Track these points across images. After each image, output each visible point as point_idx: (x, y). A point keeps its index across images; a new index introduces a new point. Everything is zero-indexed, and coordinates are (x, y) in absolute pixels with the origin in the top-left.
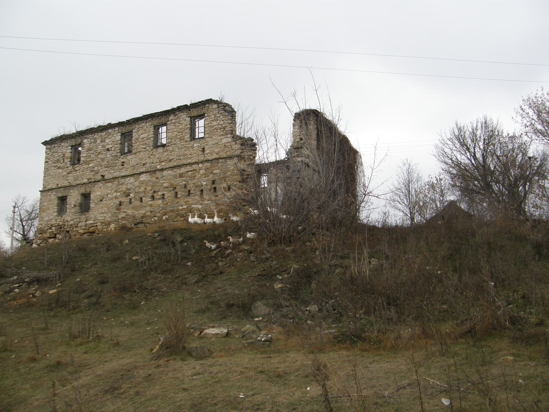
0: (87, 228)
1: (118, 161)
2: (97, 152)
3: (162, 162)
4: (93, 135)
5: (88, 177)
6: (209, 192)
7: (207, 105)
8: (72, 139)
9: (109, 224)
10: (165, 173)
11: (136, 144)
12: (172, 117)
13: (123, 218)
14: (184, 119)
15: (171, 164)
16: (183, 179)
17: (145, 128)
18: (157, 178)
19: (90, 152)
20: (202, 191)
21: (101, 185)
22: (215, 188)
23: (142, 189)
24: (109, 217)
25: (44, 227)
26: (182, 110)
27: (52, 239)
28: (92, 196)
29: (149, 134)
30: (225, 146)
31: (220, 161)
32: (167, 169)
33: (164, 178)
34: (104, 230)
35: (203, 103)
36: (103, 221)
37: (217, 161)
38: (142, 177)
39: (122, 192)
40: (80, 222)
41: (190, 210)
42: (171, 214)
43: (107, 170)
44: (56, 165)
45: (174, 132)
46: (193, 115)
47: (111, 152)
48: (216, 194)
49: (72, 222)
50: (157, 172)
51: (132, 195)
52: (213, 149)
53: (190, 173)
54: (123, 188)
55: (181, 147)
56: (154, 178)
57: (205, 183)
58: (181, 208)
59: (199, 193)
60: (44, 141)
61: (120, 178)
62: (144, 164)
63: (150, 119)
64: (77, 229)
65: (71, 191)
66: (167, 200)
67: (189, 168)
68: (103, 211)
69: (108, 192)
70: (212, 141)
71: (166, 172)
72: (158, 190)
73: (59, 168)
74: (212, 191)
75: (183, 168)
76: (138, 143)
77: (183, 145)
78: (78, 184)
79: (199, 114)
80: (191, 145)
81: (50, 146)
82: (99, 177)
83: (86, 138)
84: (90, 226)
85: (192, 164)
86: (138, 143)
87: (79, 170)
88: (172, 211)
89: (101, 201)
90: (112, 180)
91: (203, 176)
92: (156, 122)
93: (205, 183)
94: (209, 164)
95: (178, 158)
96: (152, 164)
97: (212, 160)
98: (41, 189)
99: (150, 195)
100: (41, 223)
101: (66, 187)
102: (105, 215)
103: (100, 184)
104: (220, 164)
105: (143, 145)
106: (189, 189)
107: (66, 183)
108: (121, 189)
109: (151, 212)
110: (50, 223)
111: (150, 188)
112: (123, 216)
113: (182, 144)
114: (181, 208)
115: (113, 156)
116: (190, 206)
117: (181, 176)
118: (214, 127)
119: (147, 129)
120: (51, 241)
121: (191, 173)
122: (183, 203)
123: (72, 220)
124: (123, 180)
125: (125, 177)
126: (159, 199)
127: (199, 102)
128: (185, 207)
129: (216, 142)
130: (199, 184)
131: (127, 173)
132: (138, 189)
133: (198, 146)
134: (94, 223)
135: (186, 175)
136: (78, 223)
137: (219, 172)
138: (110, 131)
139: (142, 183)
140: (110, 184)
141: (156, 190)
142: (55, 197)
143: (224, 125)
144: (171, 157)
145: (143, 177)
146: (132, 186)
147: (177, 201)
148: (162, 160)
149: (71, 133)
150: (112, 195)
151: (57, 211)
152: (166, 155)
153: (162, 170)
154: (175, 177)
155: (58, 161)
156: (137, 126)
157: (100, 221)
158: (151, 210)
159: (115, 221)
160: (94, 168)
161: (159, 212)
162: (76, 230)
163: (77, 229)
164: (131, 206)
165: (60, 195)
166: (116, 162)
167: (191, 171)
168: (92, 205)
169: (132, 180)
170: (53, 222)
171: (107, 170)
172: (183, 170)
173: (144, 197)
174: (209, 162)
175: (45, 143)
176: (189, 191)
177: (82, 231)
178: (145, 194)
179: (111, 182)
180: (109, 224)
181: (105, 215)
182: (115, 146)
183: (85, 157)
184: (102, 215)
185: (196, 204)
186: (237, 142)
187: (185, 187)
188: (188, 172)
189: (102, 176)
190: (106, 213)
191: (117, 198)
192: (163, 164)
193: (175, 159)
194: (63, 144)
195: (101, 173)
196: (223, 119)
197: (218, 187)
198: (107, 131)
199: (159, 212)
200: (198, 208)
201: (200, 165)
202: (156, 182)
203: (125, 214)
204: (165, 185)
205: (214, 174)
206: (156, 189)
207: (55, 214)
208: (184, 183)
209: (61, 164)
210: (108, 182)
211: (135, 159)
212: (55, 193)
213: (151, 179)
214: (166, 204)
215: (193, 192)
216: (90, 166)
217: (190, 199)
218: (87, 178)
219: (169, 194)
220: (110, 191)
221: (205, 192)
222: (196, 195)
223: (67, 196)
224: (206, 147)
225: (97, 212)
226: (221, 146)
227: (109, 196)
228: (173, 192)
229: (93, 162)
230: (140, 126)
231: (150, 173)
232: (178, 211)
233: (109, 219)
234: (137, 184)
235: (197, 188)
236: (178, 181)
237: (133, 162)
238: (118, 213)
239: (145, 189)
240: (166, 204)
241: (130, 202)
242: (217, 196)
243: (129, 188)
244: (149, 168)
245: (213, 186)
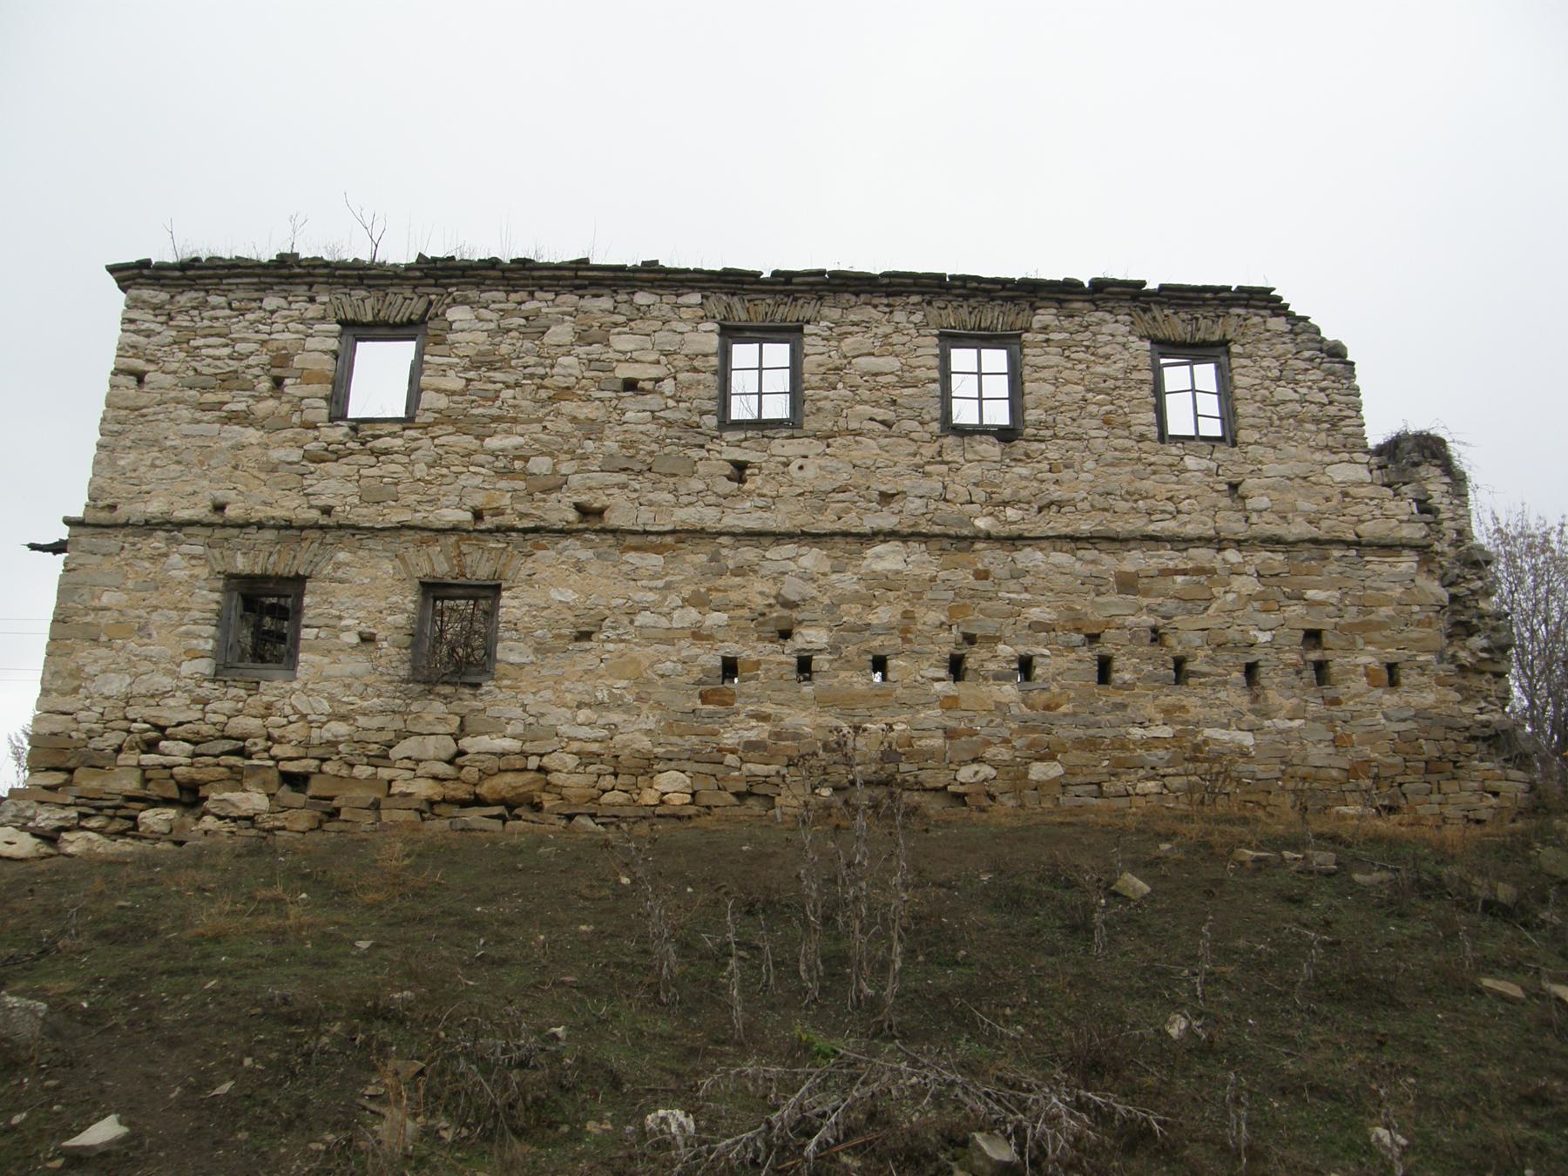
0: (470, 773)
1: (704, 453)
2: (547, 382)
3: (1006, 504)
4: (514, 297)
5: (479, 500)
6: (1293, 679)
7: (1235, 311)
8: (355, 286)
9: (647, 766)
10: (1031, 557)
11: (831, 394)
12: (1045, 316)
13: (751, 746)
14: (1121, 339)
15: (1058, 524)
16: (1145, 601)
17: (889, 329)
18: (982, 575)
19: (498, 376)
20: (1251, 670)
21: (584, 554)
22: (1320, 667)
23: (883, 615)
24: (649, 732)
25: (90, 735)
26: (1105, 300)
27: (171, 813)
28: (510, 605)
29: (914, 362)
30: (1345, 494)
31: (1336, 553)
32: (1044, 544)
33: (1028, 580)
34: (607, 798)
35: (1226, 295)
36: (595, 747)
37: (1315, 552)
38: (878, 557)
39: (746, 612)
40: (403, 735)
41: (1197, 748)
42: (1076, 757)
43: (623, 486)
44: (210, 397)
45: (1067, 382)
46: (1165, 332)
47: (652, 401)
48: (1329, 693)
49: (340, 729)
50: (979, 546)
51: (813, 637)
52: (1290, 497)
53: (1179, 579)
54: (757, 591)
55: (1109, 456)
56: (960, 573)
57: (1264, 637)
58: (1137, 732)
59: (1237, 676)
60: (132, 258)
61: (722, 540)
62: (886, 498)
63: (915, 299)
64: (385, 773)
65: (342, 556)
66: (1055, 688)
67: (1167, 557)
68: (602, 695)
69: (638, 596)
70: (1280, 461)
71: (1039, 555)
72: (991, 632)
73: (233, 418)
74: (1309, 674)
75: (1136, 554)
76: (842, 391)
77: (1124, 450)
78: (403, 527)
79: (1200, 336)
80: (1170, 460)
81: (164, 296)
82: (559, 511)
83: (465, 302)
84: (493, 763)
85: (1125, 541)
86: (842, 391)
87: (409, 452)
88: (1091, 744)
89: (585, 636)
90: (669, 539)
91: (1257, 605)
92: (954, 315)
93: (1264, 637)
94: (1280, 557)
95: (1100, 502)
96: (942, 505)
97: (1294, 543)
98: (78, 512)
99: (947, 650)
100: (68, 703)
101: (302, 528)
102: (615, 717)
103: (575, 549)
104: (1334, 567)
105: (877, 404)
106: (1178, 651)
107: (290, 506)
108: (735, 596)
109: (950, 734)
110: (150, 713)
111: (939, 616)
112: (752, 735)
113: (1119, 443)
114: (1137, 732)
115: (670, 424)
116: (1195, 734)
117: (1127, 584)
118: (625, 427)
119: (896, 338)
120: (154, 819)
121: (1186, 583)
122: (1150, 711)
123: (343, 718)
124: (748, 554)
125: (766, 541)
126: (999, 677)
127: (1205, 289)
128: (1166, 732)
129: (1301, 469)
130: (1233, 634)
131: (776, 520)
132: (856, 608)
133: (1208, 472)
134: (525, 755)
135: (1160, 584)
136: (388, 736)
137: (1334, 601)
138: (642, 298)
139: (888, 583)
140: (654, 560)
141: (978, 632)
142: (203, 572)
143: (1332, 410)
144: (1056, 493)
145: (887, 559)
146: (810, 590)
147: (1119, 700)
148: (1007, 493)
149: (349, 257)
150: (668, 615)
151: (214, 654)
152: (1022, 478)
153: (1015, 541)
154: (1096, 584)
155: (228, 381)
156: (835, 314)
157: (575, 746)
158: (952, 724)
159: (695, 756)
160: (526, 459)
161: (1006, 741)
162: (373, 778)
163: (385, 773)
164: (807, 689)
165: (241, 564)
166: (695, 454)
167: (1184, 572)
168: (510, 652)
169: (812, 558)
170: (174, 711)
171: (623, 486)
172: (1134, 561)
173: (897, 654)
174: (1278, 547)
175: (130, 275)
176: (1179, 663)
177: (423, 789)
178: (905, 640)
179: (657, 549)
180: (647, 766)
181: (615, 717)
182: (680, 376)
183: (453, 393)
184: (583, 715)
185: (1226, 726)
186: (1404, 489)
187: (1157, 636)
188: (1167, 573)
189: (578, 507)
190: (617, 703)
191: (709, 637)
192: (1011, 513)
193: (1086, 506)
194: (271, 302)
195: (577, 492)
196: (1324, 384)
197: (1337, 663)
198: (622, 297)
199: (1006, 741)
200: (1241, 747)
201: (1232, 555)
202: (974, 594)
203: (767, 727)
204: (1035, 613)
205: (1312, 604)
206: (979, 624)
207: (205, 666)
208: (1149, 620)
209: (259, 399)
210: (636, 549)
211: (822, 462)
212: (199, 550)
213: (943, 575)
214: (1047, 707)
215: (1205, 668)
216: (493, 443)
217: (1191, 700)
218: (469, 503)
219: (1063, 662)
220: (651, 596)
221: (1266, 676)
222: (1225, 683)
223: (299, 581)
224: (1250, 483)
225: (548, 694)
226: (1328, 492)
227: (643, 619)
228: (1086, 653)
229: (519, 428)
230: (853, 317)
231: (934, 544)
232: (1123, 747)
233: (645, 743)
234: (847, 582)
235: (1224, 656)
236: (1109, 604)
237: (810, 472)
238: (711, 715)
239: (908, 615)
240: (1047, 707)
241: (804, 666)
242: (1335, 702)
243: (794, 597)
244: (923, 521)
245: (1314, 655)
